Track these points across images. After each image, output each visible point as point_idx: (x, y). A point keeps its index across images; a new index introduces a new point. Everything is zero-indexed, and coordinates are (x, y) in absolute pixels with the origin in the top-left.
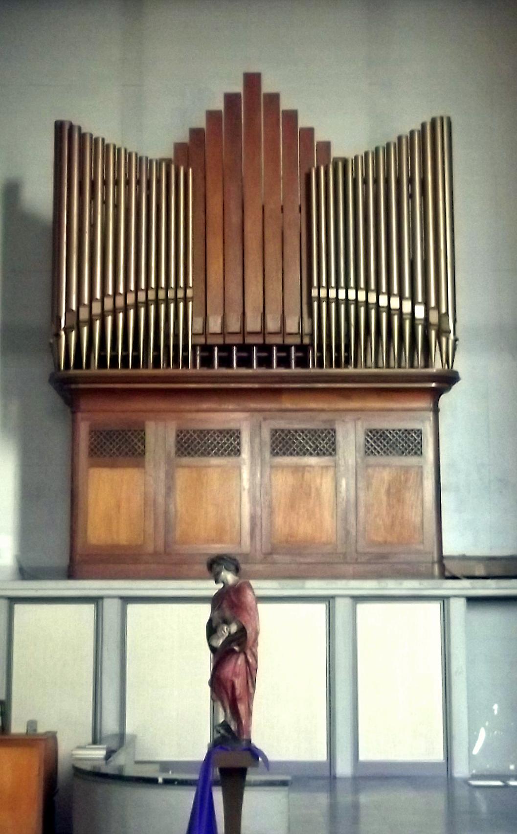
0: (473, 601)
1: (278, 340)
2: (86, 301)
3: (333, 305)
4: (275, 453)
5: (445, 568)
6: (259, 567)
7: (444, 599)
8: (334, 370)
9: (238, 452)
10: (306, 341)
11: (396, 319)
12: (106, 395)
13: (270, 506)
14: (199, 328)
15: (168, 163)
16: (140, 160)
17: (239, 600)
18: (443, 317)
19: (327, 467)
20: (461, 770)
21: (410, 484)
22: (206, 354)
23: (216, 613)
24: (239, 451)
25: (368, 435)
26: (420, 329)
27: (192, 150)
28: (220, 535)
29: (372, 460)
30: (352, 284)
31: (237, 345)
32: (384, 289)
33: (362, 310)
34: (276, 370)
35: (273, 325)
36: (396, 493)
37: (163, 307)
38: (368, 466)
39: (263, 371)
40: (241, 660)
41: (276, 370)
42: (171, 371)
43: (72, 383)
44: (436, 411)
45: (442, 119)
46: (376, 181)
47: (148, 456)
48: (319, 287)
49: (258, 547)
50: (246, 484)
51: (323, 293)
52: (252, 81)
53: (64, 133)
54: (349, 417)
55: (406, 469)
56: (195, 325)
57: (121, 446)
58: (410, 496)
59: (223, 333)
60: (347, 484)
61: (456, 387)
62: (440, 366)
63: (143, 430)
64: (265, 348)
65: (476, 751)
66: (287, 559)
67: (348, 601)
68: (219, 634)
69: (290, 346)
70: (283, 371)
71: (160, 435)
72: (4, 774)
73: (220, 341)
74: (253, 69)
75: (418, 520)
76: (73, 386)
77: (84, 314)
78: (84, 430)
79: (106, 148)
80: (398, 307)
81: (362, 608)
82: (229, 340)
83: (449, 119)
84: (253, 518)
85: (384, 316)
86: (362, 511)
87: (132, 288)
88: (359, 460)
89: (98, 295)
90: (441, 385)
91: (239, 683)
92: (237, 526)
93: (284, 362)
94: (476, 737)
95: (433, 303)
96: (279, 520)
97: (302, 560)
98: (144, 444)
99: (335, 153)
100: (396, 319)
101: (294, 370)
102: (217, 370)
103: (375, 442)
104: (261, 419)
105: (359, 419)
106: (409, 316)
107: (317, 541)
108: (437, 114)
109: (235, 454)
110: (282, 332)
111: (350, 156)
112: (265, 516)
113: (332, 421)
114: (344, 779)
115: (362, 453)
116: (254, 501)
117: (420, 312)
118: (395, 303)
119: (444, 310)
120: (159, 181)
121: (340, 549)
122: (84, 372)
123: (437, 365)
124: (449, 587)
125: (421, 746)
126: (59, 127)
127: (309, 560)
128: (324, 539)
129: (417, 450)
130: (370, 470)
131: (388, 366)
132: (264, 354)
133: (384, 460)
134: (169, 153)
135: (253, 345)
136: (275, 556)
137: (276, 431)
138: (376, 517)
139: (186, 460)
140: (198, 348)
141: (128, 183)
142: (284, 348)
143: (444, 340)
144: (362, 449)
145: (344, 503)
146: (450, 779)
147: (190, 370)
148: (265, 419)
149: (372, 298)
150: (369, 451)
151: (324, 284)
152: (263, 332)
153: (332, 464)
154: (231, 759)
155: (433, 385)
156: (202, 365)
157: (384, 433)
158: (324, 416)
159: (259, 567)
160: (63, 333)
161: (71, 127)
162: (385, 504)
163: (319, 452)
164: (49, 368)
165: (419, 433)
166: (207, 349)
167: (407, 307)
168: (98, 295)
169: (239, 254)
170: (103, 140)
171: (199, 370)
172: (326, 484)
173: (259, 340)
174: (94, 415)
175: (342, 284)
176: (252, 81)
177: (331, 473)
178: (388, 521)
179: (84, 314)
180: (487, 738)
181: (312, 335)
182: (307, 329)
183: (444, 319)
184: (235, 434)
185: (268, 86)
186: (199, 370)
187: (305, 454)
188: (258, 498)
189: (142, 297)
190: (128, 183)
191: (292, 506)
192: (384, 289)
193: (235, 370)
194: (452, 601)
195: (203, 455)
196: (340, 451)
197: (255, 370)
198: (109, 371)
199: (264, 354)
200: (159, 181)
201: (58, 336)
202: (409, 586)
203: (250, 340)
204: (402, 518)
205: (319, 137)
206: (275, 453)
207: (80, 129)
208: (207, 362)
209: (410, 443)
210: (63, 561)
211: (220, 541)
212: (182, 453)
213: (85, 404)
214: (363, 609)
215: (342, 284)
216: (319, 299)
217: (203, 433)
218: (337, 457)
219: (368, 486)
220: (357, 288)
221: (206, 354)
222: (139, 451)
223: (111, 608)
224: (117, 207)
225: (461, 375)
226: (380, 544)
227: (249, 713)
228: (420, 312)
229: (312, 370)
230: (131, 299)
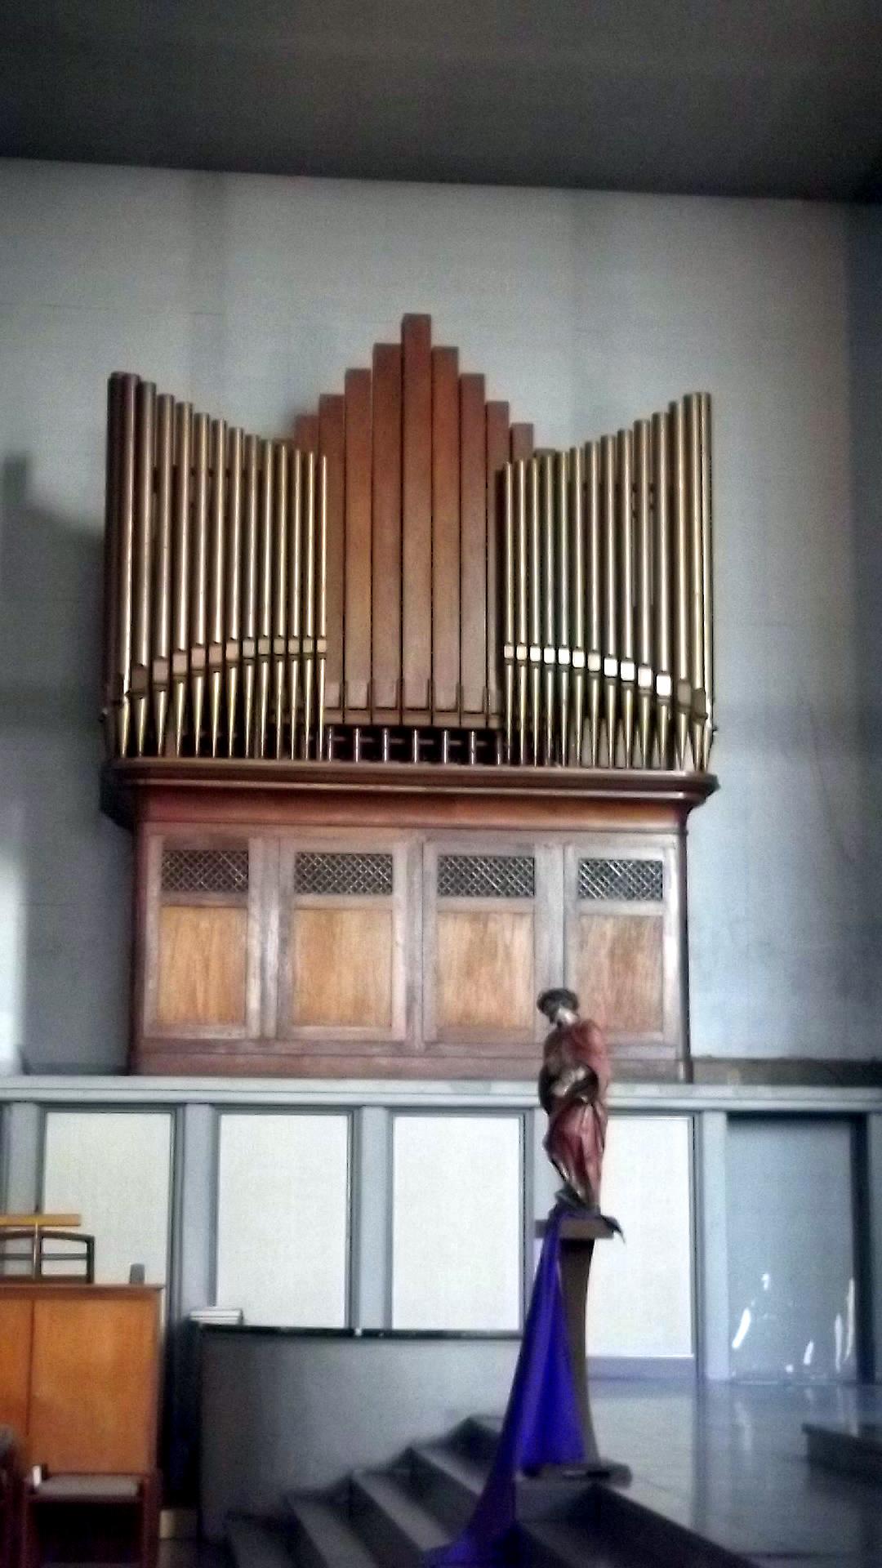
0: (737, 1118)
1: (452, 721)
2: (164, 653)
3: (536, 672)
4: (444, 890)
5: (691, 1069)
7: (695, 1114)
8: (535, 769)
9: (388, 889)
10: (494, 724)
11: (628, 696)
12: (155, 799)
13: (436, 971)
14: (333, 700)
17: (585, 1040)
18: (697, 695)
20: (718, 1369)
21: (645, 942)
23: (552, 1059)
24: (390, 886)
26: (664, 712)
27: (321, 428)
28: (360, 1009)
29: (588, 905)
31: (476, 730)
32: (612, 650)
34: (447, 766)
37: (280, 666)
38: (582, 914)
39: (427, 767)
40: (588, 1113)
41: (447, 766)
43: (140, 777)
44: (683, 834)
45: (687, 401)
47: (254, 892)
50: (400, 938)
52: (416, 327)
53: (124, 394)
54: (554, 839)
55: (638, 921)
56: (328, 695)
57: (216, 874)
58: (642, 960)
59: (370, 707)
61: (712, 800)
63: (246, 853)
64: (432, 733)
65: (737, 1343)
66: (461, 1050)
68: (565, 1080)
69: (440, 730)
70: (456, 767)
75: (655, 996)
76: (141, 782)
77: (161, 673)
79: (196, 420)
82: (379, 720)
83: (709, 398)
84: (410, 990)
85: (611, 690)
87: (234, 634)
88: (570, 905)
90: (690, 796)
91: (587, 1140)
92: (386, 998)
95: (683, 674)
96: (449, 992)
98: (246, 873)
99: (541, 441)
100: (628, 696)
101: (474, 767)
102: (358, 763)
103: (593, 879)
104: (423, 838)
105: (568, 843)
107: (506, 1025)
108: (692, 388)
109: (384, 891)
111: (563, 447)
112: (428, 986)
113: (530, 847)
115: (574, 896)
116: (411, 964)
118: (628, 671)
119: (698, 685)
123: (685, 768)
124: (704, 1095)
126: (118, 386)
128: (517, 1021)
129: (656, 891)
130: (584, 920)
132: (430, 742)
135: (355, 727)
136: (441, 1046)
137: (446, 859)
138: (593, 990)
139: (309, 899)
143: (698, 728)
147: (319, 764)
148: (429, 839)
150: (584, 893)
151: (523, 639)
152: (430, 709)
155: (680, 795)
160: (126, 700)
161: (140, 388)
163: (508, 892)
168: (182, 644)
171: (331, 763)
172: (519, 939)
173: (423, 720)
176: (416, 327)
177: (526, 923)
178: (610, 996)
180: (753, 1326)
181: (502, 715)
182: (494, 706)
184: (385, 861)
185: (441, 336)
186: (331, 763)
188: (418, 958)
192: (612, 650)
193: (387, 764)
195: (335, 891)
197: (416, 765)
199: (430, 742)
201: (118, 704)
203: (410, 720)
206: (444, 890)
208: (344, 751)
209: (644, 881)
211: (359, 1022)
212: (305, 888)
216: (515, 661)
219: (582, 945)
220: (572, 647)
222: (239, 882)
223: (198, 1119)
225: (720, 782)
227: (599, 1175)
228: (664, 686)
229: (500, 768)
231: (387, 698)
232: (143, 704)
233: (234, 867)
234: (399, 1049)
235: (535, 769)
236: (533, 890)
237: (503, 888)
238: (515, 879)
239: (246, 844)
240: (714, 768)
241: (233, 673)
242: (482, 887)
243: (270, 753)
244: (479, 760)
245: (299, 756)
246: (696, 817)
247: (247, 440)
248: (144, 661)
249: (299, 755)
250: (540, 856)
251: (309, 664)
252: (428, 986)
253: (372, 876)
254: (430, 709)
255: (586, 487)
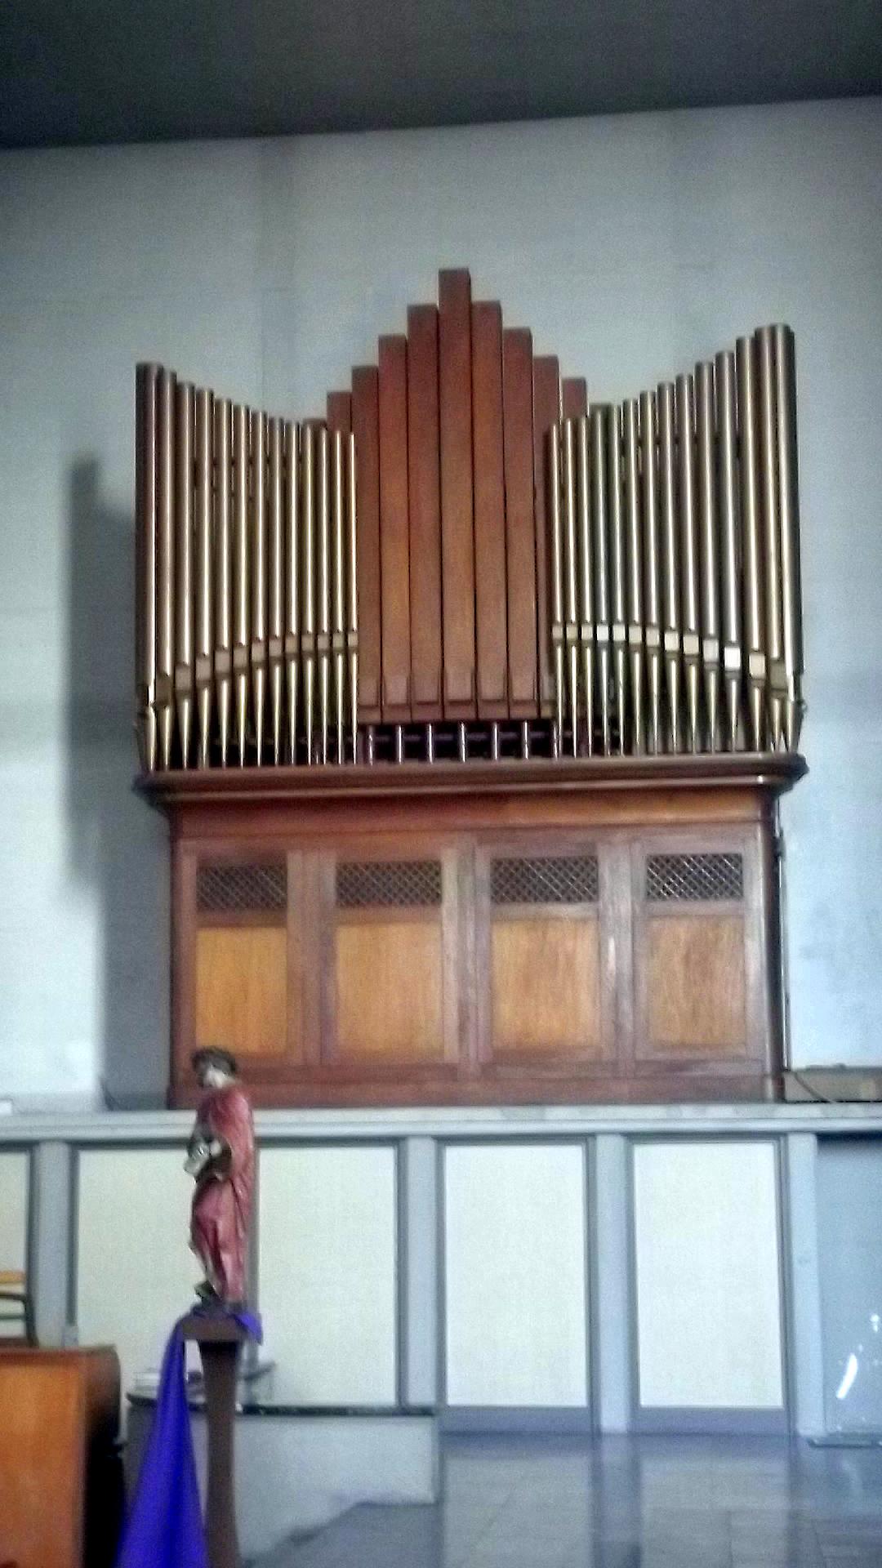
0: (827, 1139)
6: (472, 1087)
7: (777, 1137)
8: (592, 760)
9: (436, 898)
10: (546, 712)
11: (693, 673)
14: (370, 697)
15: (324, 424)
16: (269, 423)
19: (584, 921)
20: (812, 1424)
22: (538, 735)
25: (652, 866)
26: (734, 687)
27: (358, 405)
29: (658, 906)
30: (620, 615)
33: (637, 658)
35: (491, 688)
36: (700, 961)
37: (325, 662)
38: (653, 917)
42: (326, 767)
44: (768, 822)
46: (677, 441)
48: (595, 622)
49: (472, 1054)
51: (587, 633)
52: (455, 282)
54: (620, 836)
57: (247, 893)
60: (617, 949)
62: (783, 749)
64: (479, 726)
65: (842, 1393)
67: (619, 1142)
71: (311, 871)
72: (36, 1414)
73: (405, 717)
74: (454, 261)
75: (736, 1005)
78: (188, 868)
80: (696, 650)
81: (641, 1152)
82: (419, 715)
83: (789, 337)
84: (463, 1007)
85: (673, 667)
86: (643, 988)
89: (206, 648)
92: (437, 1016)
93: (511, 748)
94: (841, 1372)
96: (506, 1009)
97: (545, 1074)
102: (557, 759)
103: (663, 877)
105: (635, 839)
106: (716, 667)
108: (765, 323)
110: (507, 699)
111: (616, 402)
112: (481, 1005)
113: (593, 846)
114: (613, 1435)
117: (733, 659)
118: (691, 645)
119: (775, 654)
120: (301, 459)
121: (607, 1055)
122: (185, 773)
124: (784, 1117)
125: (747, 1384)
126: (143, 373)
127: (555, 1075)
128: (581, 1039)
130: (655, 924)
131: (665, 750)
133: (678, 906)
134: (320, 411)
138: (666, 1002)
140: (371, 730)
141: (251, 461)
142: (511, 725)
144: (642, 886)
145: (612, 980)
146: (793, 1437)
147: (355, 767)
149: (653, 638)
150: (654, 892)
152: (475, 701)
153: (591, 914)
154: (221, 1331)
155: (761, 779)
156: (378, 755)
157: (678, 862)
158: (580, 837)
159: (472, 1087)
160: (151, 712)
162: (680, 976)
164: (132, 770)
165: (737, 860)
166: (385, 730)
167: (711, 651)
168: (206, 648)
169: (434, 570)
170: (212, 395)
172: (583, 948)
173: (501, 713)
174: (227, 842)
175: (604, 617)
176: (455, 282)
179: (184, 680)
181: (554, 703)
183: (775, 669)
185: (480, 293)
187: (547, 899)
188: (471, 971)
189: (275, 649)
190: (251, 461)
191: (527, 982)
194: (792, 1139)
196: (605, 894)
198: (225, 772)
200: (301, 459)
201: (144, 716)
202: (719, 1116)
204: (711, 1001)
205: (566, 371)
207: (174, 376)
208: (386, 752)
209: (715, 878)
210: (159, 1082)
213: (187, 826)
214: (644, 1154)
215: (604, 617)
217: (378, 868)
218: (601, 904)
221: (538, 735)
223: (420, 1154)
224: (251, 500)
226: (673, 1047)
228: (733, 659)
229: (557, 759)
230: (258, 653)
231: (429, 692)
232: (168, 713)
233: (272, 883)
234: (450, 1072)
235: (269, 772)
236: (596, 892)
237: (563, 892)
238: (576, 880)
239: (285, 859)
240: (804, 750)
241: (260, 675)
242: (541, 893)
243: (598, 749)
244: (534, 751)
245: (284, 761)
246: (789, 804)
247: (252, 419)
248: (168, 669)
249: (629, 750)
250: (295, 863)
251: (340, 660)
252: (481, 1005)
253: (417, 887)
254: (475, 701)
255: (697, 440)
